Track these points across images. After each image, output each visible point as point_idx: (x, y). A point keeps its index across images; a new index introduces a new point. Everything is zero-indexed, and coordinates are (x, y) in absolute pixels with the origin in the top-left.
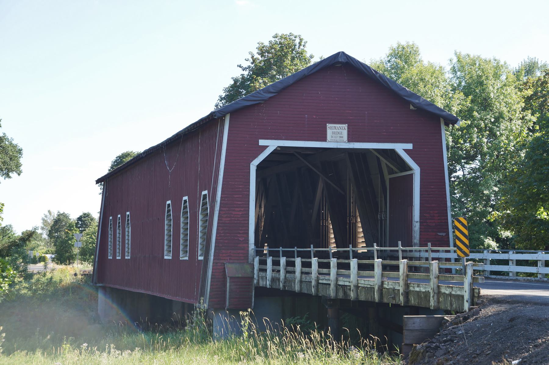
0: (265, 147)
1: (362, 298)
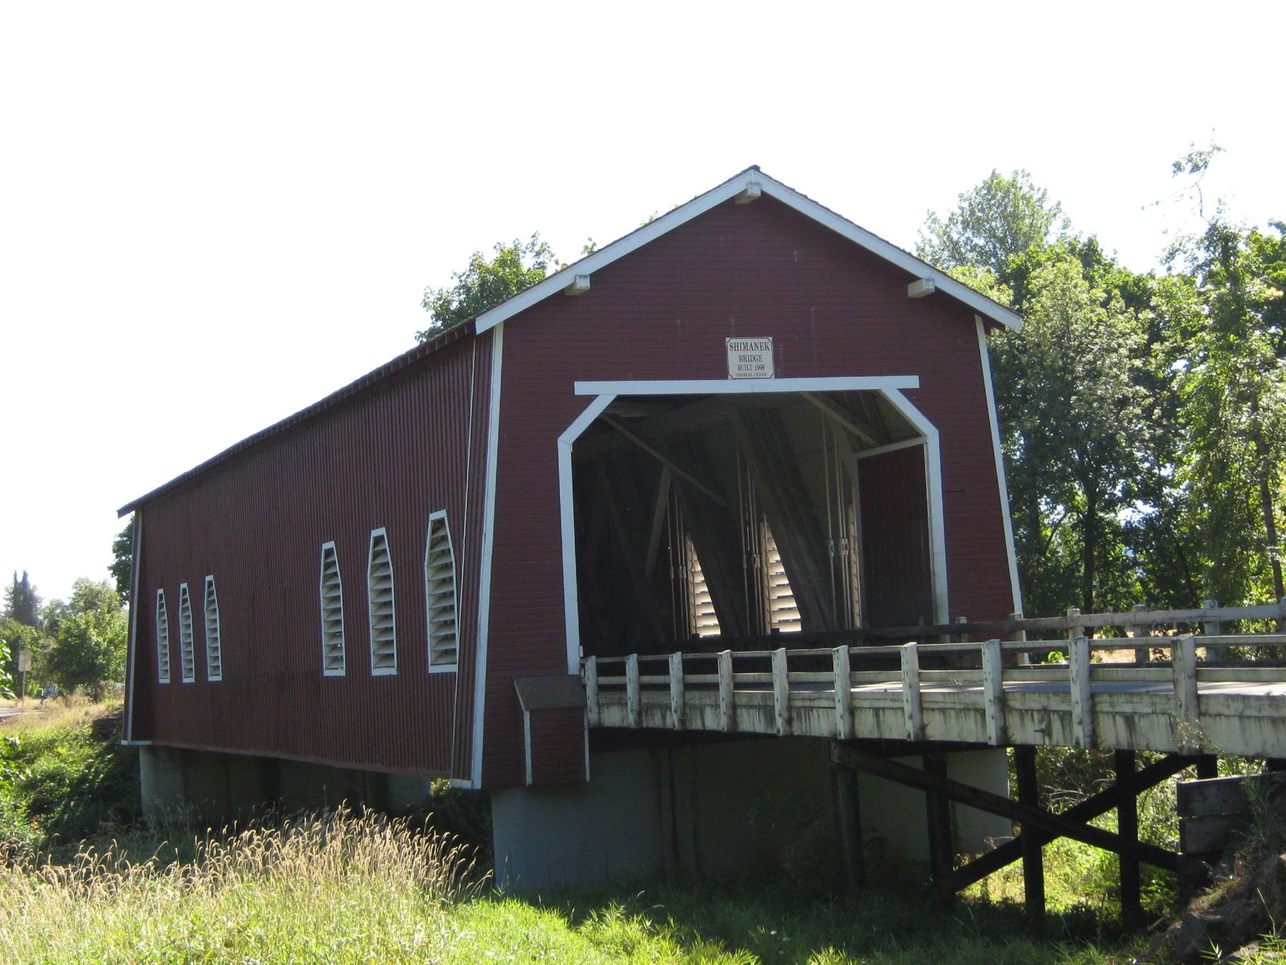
0: (589, 399)
1: (866, 728)
